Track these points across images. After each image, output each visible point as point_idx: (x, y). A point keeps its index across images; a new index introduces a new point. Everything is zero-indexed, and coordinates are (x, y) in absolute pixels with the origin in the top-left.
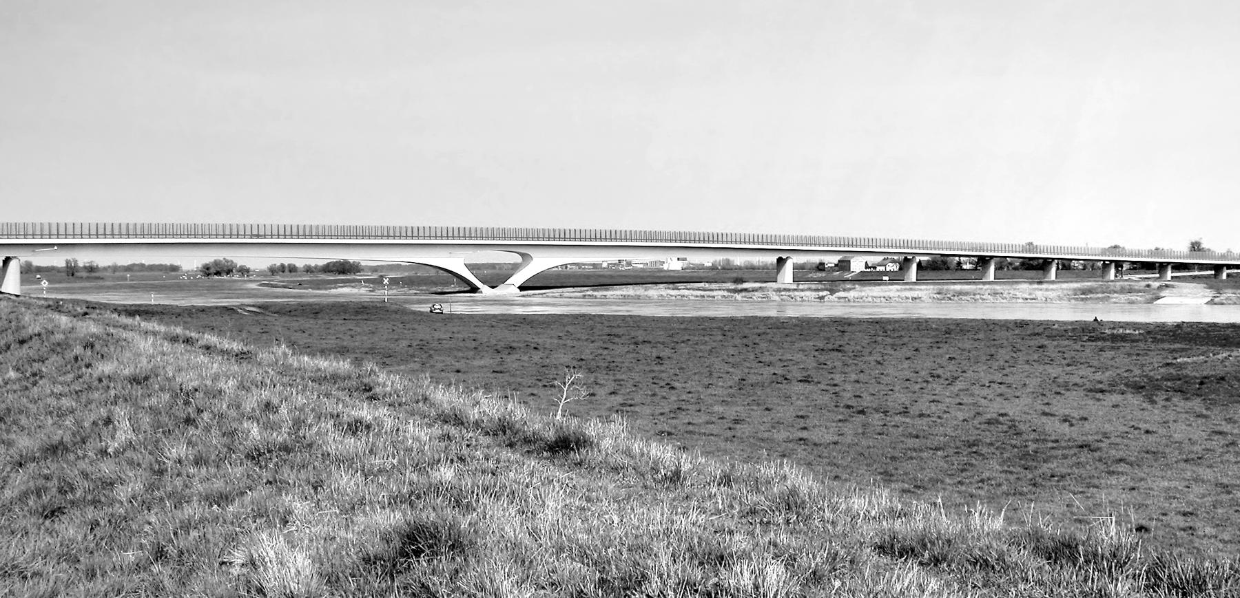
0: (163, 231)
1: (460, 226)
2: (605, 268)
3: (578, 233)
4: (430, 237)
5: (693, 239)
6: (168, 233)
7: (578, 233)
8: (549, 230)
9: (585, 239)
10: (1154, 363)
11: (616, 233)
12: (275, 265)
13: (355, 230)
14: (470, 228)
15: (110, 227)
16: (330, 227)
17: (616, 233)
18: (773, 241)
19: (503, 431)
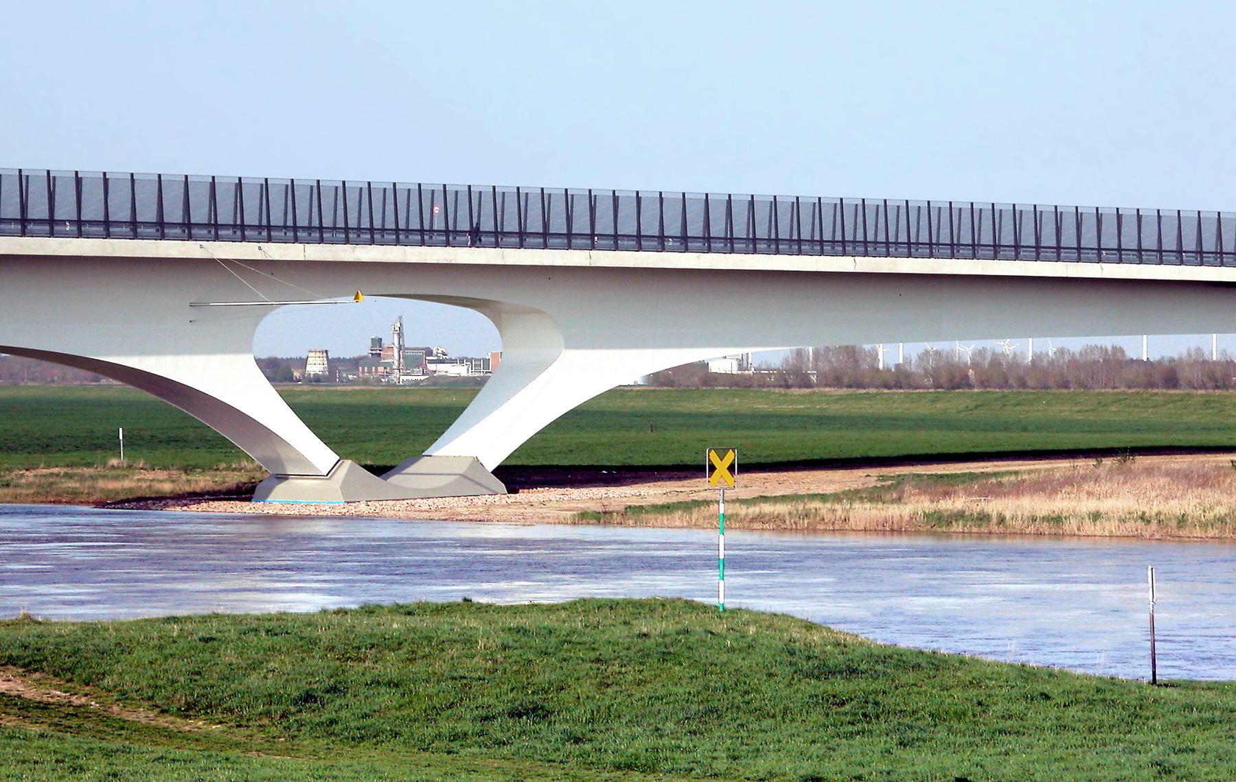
0: (569, 219)
1: (1003, 209)
2: (317, 379)
3: (628, 210)
4: (1099, 249)
5: (987, 238)
6: (327, 222)
7: (628, 210)
8: (1058, 216)
9: (79, 223)
10: (373, 558)
11: (592, 209)
12: (786, 360)
13: (903, 222)
14: (239, 185)
15: (723, 209)
16: (317, 189)
17: (592, 209)
18: (762, 232)
19: (636, 616)
